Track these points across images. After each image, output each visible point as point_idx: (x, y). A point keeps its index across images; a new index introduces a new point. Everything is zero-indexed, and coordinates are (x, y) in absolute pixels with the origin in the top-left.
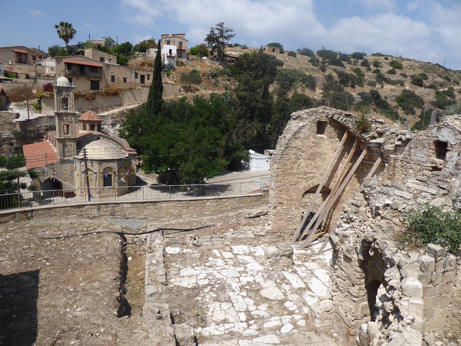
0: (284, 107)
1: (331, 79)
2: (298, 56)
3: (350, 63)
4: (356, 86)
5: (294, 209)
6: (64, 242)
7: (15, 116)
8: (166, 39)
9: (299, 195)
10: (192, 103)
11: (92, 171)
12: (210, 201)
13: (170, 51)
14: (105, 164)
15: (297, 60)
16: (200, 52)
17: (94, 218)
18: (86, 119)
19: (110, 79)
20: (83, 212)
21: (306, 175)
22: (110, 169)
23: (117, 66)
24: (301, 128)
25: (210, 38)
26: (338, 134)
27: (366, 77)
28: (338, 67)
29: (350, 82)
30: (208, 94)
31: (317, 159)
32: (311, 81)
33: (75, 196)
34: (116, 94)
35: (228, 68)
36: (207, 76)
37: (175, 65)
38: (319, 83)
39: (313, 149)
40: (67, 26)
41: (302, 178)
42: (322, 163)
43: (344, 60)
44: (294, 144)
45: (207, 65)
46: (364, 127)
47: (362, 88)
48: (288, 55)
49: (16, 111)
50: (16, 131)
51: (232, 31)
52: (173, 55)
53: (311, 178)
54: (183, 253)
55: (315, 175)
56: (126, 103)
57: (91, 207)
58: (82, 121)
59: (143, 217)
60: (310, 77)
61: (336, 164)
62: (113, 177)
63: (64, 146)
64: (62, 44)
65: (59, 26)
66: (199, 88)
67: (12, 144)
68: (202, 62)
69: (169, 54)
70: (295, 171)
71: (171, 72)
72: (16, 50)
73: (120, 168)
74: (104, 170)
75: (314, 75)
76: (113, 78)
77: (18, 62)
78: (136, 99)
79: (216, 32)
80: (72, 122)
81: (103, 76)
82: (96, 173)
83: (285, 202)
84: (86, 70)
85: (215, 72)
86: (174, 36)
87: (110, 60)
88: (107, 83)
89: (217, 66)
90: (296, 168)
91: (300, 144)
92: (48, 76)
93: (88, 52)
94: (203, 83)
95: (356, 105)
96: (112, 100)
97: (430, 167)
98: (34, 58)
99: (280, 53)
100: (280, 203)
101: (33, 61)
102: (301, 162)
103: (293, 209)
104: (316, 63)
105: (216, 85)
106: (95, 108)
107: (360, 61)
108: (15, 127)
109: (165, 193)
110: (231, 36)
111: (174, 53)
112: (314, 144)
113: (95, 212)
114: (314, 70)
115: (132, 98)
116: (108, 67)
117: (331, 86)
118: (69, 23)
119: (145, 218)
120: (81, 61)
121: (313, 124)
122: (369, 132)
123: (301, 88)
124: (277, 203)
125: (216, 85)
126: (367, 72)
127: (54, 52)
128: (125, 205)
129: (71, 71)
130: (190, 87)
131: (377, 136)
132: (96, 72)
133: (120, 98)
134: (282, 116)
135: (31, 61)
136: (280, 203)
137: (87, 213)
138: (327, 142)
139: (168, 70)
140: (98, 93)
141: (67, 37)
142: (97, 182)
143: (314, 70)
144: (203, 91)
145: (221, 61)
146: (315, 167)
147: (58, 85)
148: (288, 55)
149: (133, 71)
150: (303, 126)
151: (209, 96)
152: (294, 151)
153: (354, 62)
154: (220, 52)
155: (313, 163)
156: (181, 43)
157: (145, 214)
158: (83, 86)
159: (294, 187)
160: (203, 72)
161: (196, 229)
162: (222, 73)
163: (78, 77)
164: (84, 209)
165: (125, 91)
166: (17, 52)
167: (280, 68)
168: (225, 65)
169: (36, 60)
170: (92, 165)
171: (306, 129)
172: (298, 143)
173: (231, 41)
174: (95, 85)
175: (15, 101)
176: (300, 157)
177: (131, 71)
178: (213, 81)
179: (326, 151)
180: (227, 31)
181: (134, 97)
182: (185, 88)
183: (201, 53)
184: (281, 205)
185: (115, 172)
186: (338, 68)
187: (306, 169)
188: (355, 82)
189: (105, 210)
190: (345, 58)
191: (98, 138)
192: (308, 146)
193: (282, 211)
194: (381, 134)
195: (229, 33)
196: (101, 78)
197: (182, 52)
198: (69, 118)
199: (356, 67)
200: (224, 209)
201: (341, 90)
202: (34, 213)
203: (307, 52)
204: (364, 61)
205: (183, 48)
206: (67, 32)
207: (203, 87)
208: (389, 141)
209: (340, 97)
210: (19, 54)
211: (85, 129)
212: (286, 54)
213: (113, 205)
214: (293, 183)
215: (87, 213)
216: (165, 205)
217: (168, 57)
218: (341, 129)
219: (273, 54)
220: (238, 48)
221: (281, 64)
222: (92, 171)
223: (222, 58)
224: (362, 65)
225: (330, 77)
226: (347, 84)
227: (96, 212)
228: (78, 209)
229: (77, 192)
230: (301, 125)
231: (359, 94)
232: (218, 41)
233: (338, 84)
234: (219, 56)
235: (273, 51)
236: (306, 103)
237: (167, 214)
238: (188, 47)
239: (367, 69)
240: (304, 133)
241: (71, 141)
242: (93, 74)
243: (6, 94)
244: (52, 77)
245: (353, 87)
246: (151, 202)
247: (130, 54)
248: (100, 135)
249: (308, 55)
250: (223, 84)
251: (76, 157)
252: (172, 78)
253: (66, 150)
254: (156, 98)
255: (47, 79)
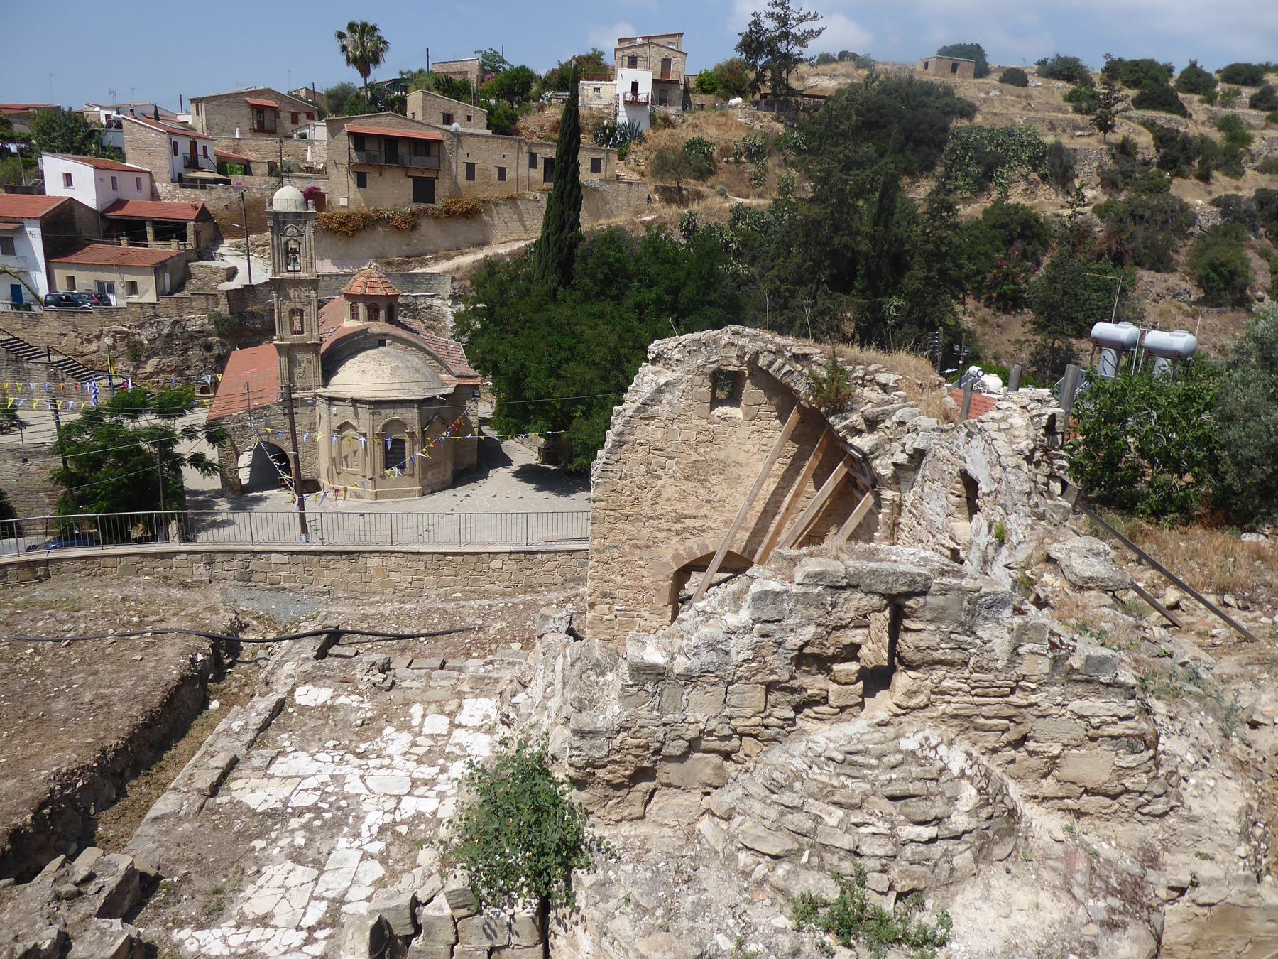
0: (943, 249)
1: (1129, 154)
2: (1035, 81)
3: (1211, 99)
4: (1215, 173)
5: (646, 614)
6: (64, 652)
7: (223, 275)
8: (627, 52)
9: (662, 577)
10: (677, 236)
11: (356, 429)
12: (500, 557)
13: (635, 86)
14: (388, 411)
15: (1028, 97)
16: (724, 83)
17: (195, 585)
18: (359, 291)
19: (462, 171)
20: (171, 567)
21: (680, 522)
22: (401, 424)
23: (487, 136)
24: (660, 390)
25: (753, 43)
26: (778, 409)
27: (1257, 145)
28: (1163, 114)
29: (1196, 163)
30: (724, 210)
31: (713, 479)
32: (1057, 161)
33: (318, 489)
34: (471, 213)
35: (800, 129)
36: (734, 155)
37: (645, 127)
38: (1087, 169)
39: (702, 450)
40: (364, 30)
41: (669, 530)
42: (728, 491)
43: (1193, 90)
44: (639, 435)
45: (741, 119)
46: (836, 396)
47: (1234, 183)
48: (1002, 80)
49: (231, 261)
50: (219, 314)
51: (815, 17)
52: (641, 98)
53: (695, 532)
54: (332, 706)
55: (709, 524)
56: (498, 236)
57: (190, 557)
58: (348, 296)
59: (320, 588)
60: (1057, 148)
61: (774, 493)
62: (407, 445)
63: (292, 363)
64: (354, 78)
65: (346, 32)
66: (704, 189)
67: (209, 348)
68: (723, 115)
69: (629, 96)
70: (646, 510)
71: (633, 146)
72: (252, 101)
73: (426, 423)
74: (385, 427)
75: (1066, 141)
76: (470, 168)
77: (255, 131)
78: (525, 227)
79: (769, 24)
80: (310, 303)
81: (444, 166)
82: (365, 435)
83: (620, 593)
84: (403, 149)
85: (758, 143)
86: (649, 40)
87: (469, 118)
88: (456, 184)
89: (770, 123)
90: (649, 501)
91: (659, 434)
92: (310, 169)
93: (415, 100)
94: (723, 177)
95: (1201, 238)
96: (463, 230)
97: (948, 548)
98: (295, 119)
99: (976, 76)
100: (605, 595)
101: (293, 127)
102: (663, 486)
103: (643, 613)
104: (1084, 105)
105: (757, 180)
106: (416, 253)
107: (1248, 92)
108: (217, 305)
109: (546, 493)
110: (812, 34)
111: (646, 90)
112: (701, 437)
113: (201, 571)
114: (1077, 128)
115: (515, 224)
116: (459, 141)
117: (1127, 175)
118: (371, 23)
119: (324, 593)
120: (389, 126)
121: (698, 380)
122: (847, 411)
123: (1023, 185)
124: (598, 593)
125: (757, 180)
126: (1266, 127)
127: (338, 104)
128: (274, 558)
129: (363, 154)
130: (680, 189)
131: (864, 427)
132: (428, 154)
133: (484, 224)
134: (933, 274)
135: (287, 124)
136: (605, 595)
137: (181, 570)
138: (743, 432)
139: (625, 140)
140: (425, 211)
141: (364, 62)
142: (368, 459)
143: (1077, 128)
144: (716, 202)
145: (780, 109)
146: (707, 501)
147: (275, 208)
148: (1002, 80)
149: (525, 149)
150: (667, 384)
151: (730, 216)
152: (641, 454)
153: (1223, 96)
154: (779, 83)
155: (702, 491)
156: (666, 63)
157: (327, 580)
158: (393, 193)
159: (646, 554)
160: (722, 143)
161: (427, 635)
162: (779, 145)
163: (381, 170)
164: (175, 560)
165: (497, 205)
166: (253, 106)
167: (965, 123)
168: (791, 122)
169: (300, 124)
170: (357, 415)
171: (678, 394)
172: (653, 431)
173: (813, 48)
174: (424, 190)
175: (234, 234)
176: (661, 472)
177: (520, 149)
178: (752, 168)
179: (742, 457)
180: (802, 20)
181: (521, 219)
182: (663, 191)
183: (726, 87)
184: (609, 600)
185: (412, 434)
186: (1162, 117)
187: (679, 505)
188: (1213, 163)
189: (225, 565)
190: (1196, 80)
191: (382, 343)
192: (684, 442)
193: (611, 616)
194: (872, 424)
195: (806, 26)
196: (438, 171)
197: (668, 86)
198: (303, 292)
199: (1228, 111)
200: (544, 580)
201: (1158, 189)
202: (51, 567)
203: (1065, 70)
204: (1262, 93)
205: (673, 77)
206: (364, 46)
207: (718, 187)
208: (887, 447)
209: (1148, 213)
210: (259, 110)
211: (354, 316)
212: (993, 79)
213: (244, 556)
214: (640, 543)
215: (181, 570)
216: (377, 561)
217: (626, 103)
218: (782, 395)
219: (952, 80)
220: (842, 68)
221: (968, 110)
222: (356, 429)
223: (782, 99)
224: (1255, 103)
225: (1125, 149)
226: (1185, 168)
227: (202, 570)
228: (158, 562)
229: (323, 481)
230: (662, 381)
231: (1216, 203)
232: (773, 51)
233: (1154, 169)
234: (774, 94)
235: (954, 68)
236: (1028, 233)
237: (383, 584)
238: (690, 67)
239: (1268, 118)
240: (670, 404)
241: (308, 352)
242: (418, 161)
243: (212, 218)
244: (319, 171)
245: (1205, 178)
246: (340, 553)
247: (527, 100)
248: (385, 334)
249: (1069, 78)
250: (779, 177)
251: (321, 390)
252: (632, 164)
253: (297, 371)
254: (562, 228)
255: (306, 178)
